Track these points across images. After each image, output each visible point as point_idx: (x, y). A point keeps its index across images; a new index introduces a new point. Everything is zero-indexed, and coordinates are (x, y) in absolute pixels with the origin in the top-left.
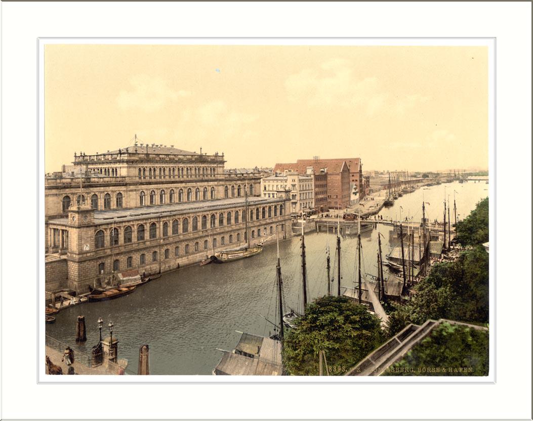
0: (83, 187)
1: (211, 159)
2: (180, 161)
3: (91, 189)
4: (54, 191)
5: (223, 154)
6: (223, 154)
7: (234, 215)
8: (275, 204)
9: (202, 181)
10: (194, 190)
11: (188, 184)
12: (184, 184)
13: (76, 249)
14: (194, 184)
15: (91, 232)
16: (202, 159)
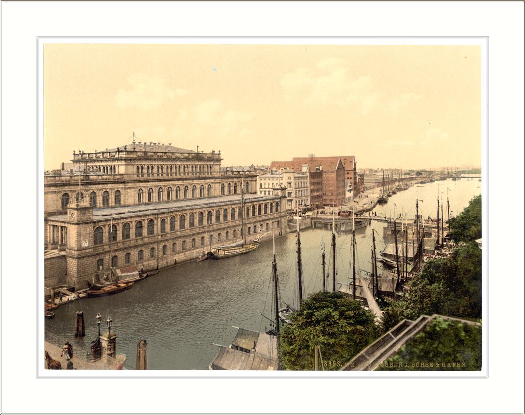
0: (82, 185)
1: (208, 157)
2: (178, 159)
3: (90, 186)
4: (53, 189)
5: (220, 151)
6: (220, 151)
7: (230, 212)
8: (271, 201)
9: (199, 178)
10: (191, 187)
11: (185, 181)
12: (181, 181)
13: (75, 245)
14: (191, 181)
16: (199, 157)
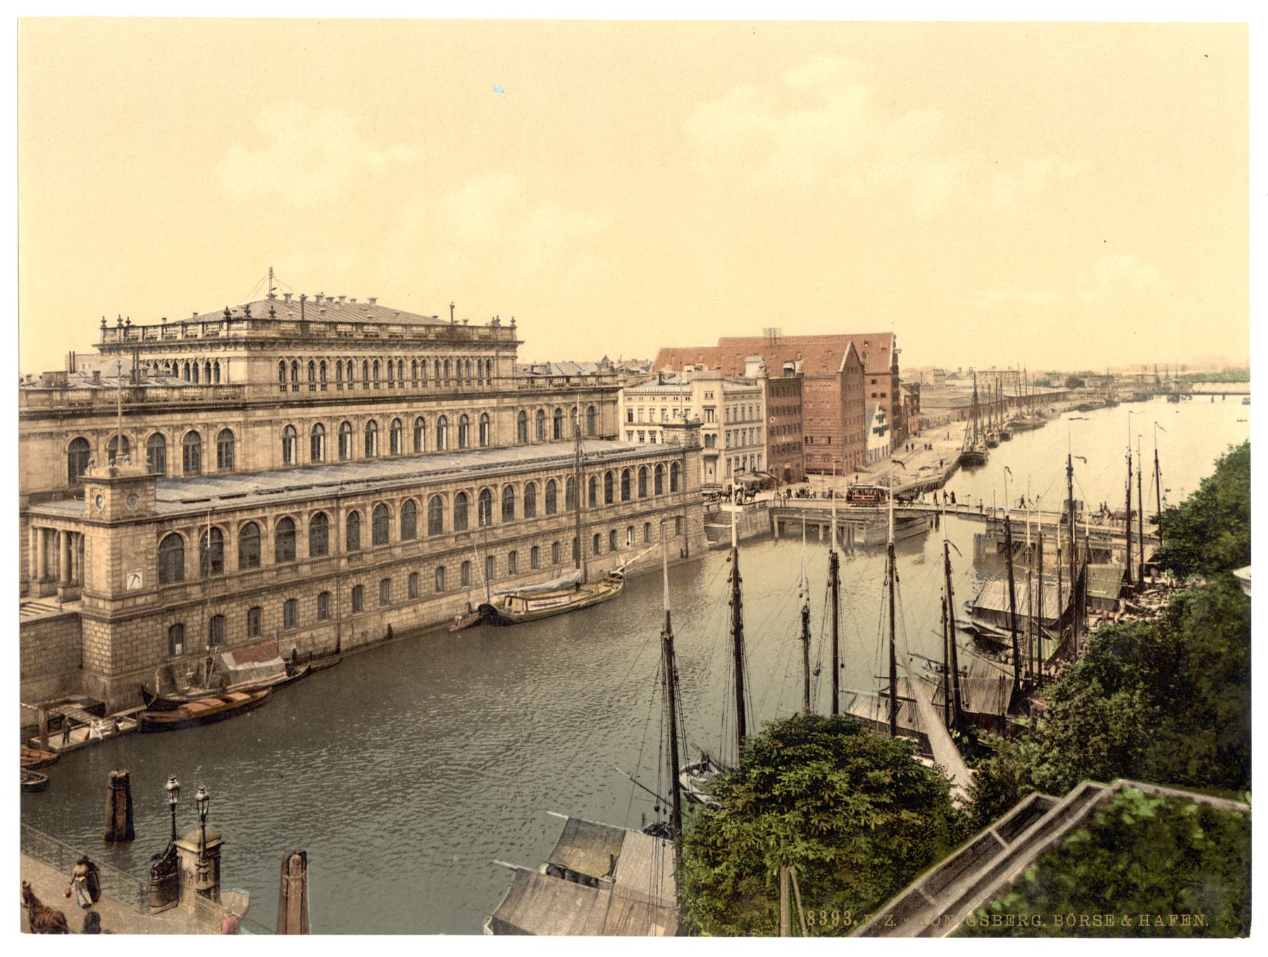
2: (395, 342)
3: (148, 418)
4: (45, 426)
5: (513, 321)
6: (513, 321)
8: (658, 460)
9: (456, 396)
10: (432, 422)
11: (415, 404)
14: (433, 405)
15: (148, 538)
16: (454, 336)
